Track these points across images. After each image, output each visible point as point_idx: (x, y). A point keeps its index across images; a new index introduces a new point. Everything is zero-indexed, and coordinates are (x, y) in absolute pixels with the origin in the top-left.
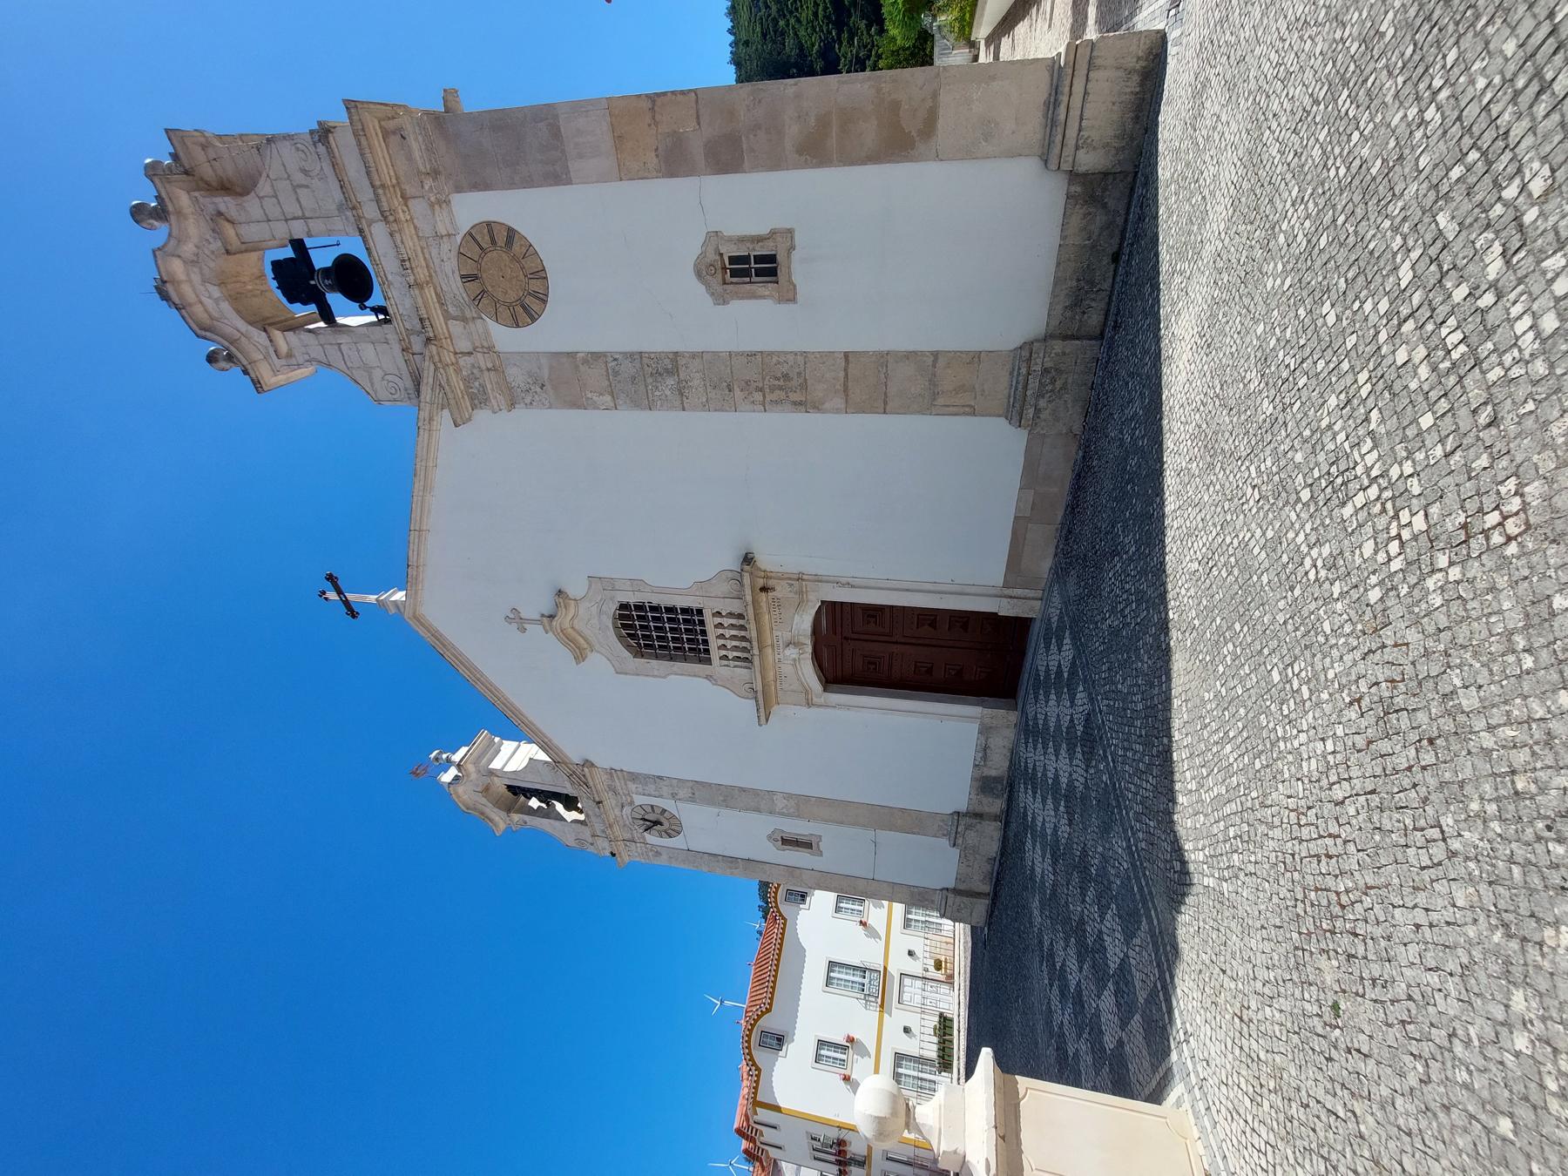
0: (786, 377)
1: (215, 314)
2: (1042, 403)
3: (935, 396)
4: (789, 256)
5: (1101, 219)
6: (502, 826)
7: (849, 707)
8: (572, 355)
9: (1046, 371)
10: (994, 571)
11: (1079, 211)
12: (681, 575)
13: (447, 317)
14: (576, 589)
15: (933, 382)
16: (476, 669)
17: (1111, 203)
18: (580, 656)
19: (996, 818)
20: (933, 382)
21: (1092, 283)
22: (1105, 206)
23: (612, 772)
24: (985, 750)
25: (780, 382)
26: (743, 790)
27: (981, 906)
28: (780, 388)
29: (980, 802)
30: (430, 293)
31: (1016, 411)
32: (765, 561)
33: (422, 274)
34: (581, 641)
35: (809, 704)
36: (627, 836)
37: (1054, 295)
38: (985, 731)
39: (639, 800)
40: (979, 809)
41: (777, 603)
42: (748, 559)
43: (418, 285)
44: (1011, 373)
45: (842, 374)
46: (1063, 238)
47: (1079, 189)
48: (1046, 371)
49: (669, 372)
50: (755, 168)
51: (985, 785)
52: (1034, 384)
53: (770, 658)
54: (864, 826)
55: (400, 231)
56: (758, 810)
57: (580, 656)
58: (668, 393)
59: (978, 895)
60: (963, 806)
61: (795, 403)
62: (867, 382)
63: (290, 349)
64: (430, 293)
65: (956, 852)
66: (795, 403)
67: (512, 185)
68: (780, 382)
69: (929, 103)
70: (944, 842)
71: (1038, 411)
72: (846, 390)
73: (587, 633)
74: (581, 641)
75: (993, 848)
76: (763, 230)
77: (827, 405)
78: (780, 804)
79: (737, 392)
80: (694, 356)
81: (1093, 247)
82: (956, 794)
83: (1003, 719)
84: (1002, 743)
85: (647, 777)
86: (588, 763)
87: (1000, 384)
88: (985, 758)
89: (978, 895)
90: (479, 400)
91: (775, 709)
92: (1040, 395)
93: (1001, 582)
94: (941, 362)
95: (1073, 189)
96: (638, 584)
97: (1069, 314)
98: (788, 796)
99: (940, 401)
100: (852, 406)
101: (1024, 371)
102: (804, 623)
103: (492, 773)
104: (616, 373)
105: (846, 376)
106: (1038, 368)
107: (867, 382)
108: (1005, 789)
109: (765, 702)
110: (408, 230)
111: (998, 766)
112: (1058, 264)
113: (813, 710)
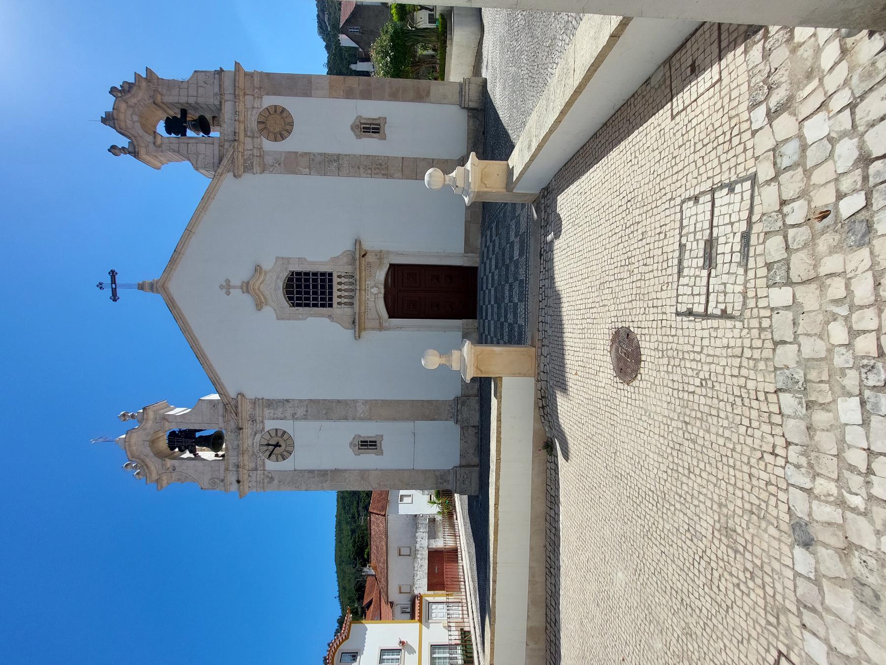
0: (381, 164)
5: (478, 123)
7: (400, 328)
8: (296, 153)
10: (458, 246)
11: (471, 120)
12: (320, 254)
13: (246, 136)
14: (267, 265)
16: (188, 324)
18: (259, 306)
23: (254, 402)
26: (339, 401)
32: (366, 246)
35: (381, 328)
39: (270, 425)
54: (408, 419)
56: (346, 418)
57: (259, 306)
63: (161, 144)
68: (379, 167)
85: (279, 401)
90: (248, 168)
96: (301, 260)
98: (366, 402)
102: (381, 275)
103: (165, 418)
104: (313, 160)
110: (242, 104)
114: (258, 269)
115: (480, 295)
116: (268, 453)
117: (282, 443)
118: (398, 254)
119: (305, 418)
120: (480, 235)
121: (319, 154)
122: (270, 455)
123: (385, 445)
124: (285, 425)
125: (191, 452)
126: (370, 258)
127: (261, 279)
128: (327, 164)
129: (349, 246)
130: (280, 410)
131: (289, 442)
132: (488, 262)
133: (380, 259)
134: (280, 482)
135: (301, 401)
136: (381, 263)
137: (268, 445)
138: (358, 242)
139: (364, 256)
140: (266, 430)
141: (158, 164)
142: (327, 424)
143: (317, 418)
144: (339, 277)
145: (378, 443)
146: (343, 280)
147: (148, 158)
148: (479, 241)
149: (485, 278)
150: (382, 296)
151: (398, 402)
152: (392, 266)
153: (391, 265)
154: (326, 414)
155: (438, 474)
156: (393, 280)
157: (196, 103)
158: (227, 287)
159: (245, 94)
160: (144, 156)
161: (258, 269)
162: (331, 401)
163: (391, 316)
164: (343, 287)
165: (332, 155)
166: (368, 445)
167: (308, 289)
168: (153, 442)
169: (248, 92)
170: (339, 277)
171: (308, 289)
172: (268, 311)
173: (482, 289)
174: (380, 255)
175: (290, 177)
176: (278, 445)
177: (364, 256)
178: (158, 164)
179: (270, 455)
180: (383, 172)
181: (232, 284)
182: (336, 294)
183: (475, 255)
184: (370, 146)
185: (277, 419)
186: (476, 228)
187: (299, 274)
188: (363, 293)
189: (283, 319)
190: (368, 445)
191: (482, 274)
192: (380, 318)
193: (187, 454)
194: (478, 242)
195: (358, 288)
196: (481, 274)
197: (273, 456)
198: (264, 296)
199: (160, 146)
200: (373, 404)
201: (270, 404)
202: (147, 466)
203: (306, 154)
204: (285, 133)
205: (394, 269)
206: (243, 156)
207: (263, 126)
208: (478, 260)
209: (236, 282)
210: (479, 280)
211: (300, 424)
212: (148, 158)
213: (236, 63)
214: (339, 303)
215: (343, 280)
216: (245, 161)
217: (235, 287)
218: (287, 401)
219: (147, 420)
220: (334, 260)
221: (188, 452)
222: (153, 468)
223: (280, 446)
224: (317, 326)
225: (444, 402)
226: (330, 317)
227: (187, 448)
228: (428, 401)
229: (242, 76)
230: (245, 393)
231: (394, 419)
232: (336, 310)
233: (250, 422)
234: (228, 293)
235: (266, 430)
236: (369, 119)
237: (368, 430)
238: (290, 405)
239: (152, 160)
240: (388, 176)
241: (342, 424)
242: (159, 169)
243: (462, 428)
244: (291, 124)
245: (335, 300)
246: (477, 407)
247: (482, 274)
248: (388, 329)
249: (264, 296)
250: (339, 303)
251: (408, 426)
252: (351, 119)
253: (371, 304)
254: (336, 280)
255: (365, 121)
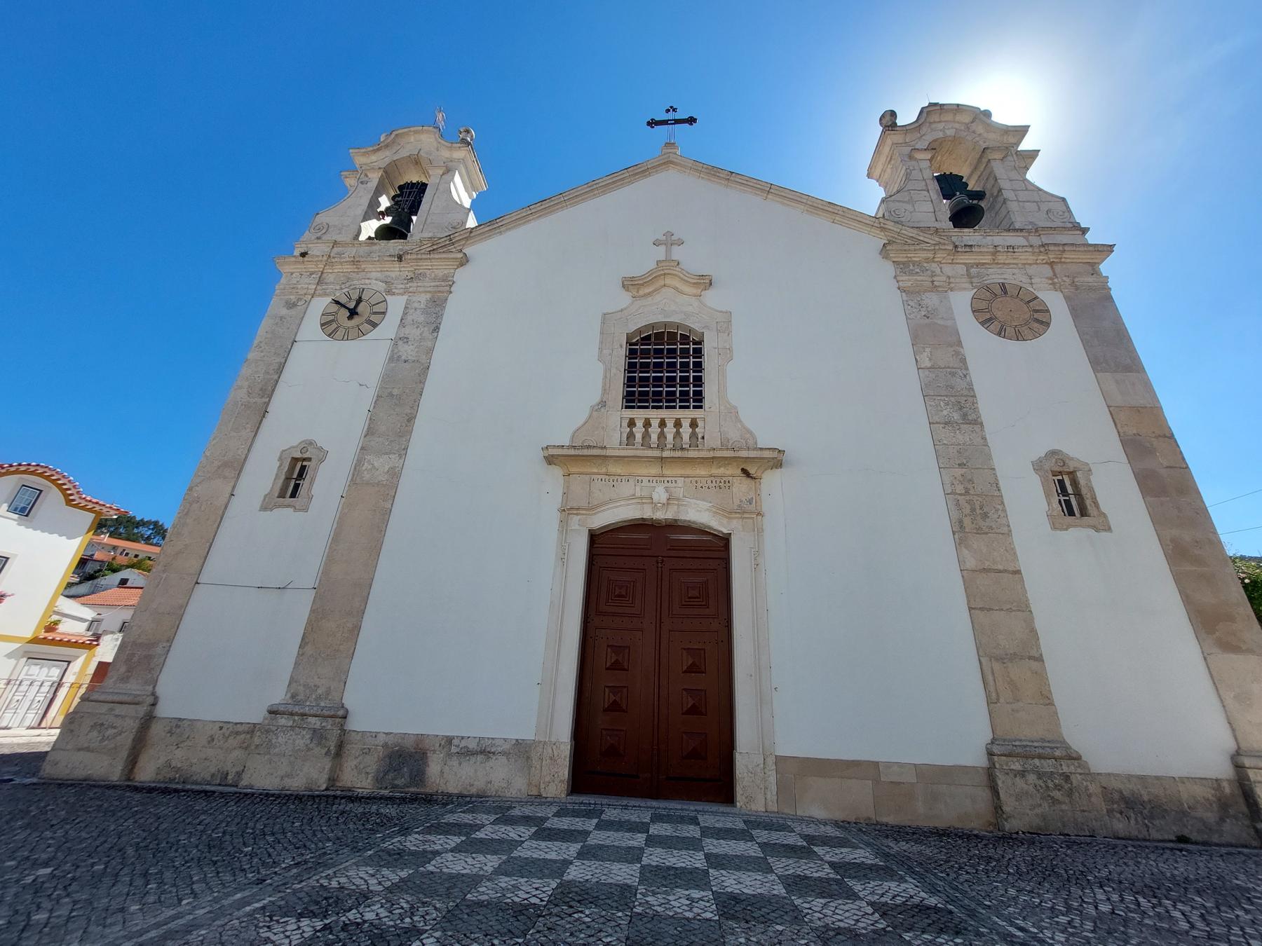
0: (985, 516)
1: (933, 126)
2: (1032, 778)
3: (993, 658)
4: (1089, 526)
5: (1211, 817)
6: (360, 160)
7: (563, 559)
8: (960, 343)
9: (1067, 778)
10: (792, 745)
11: (1209, 793)
12: (742, 390)
13: (969, 266)
14: (712, 298)
15: (1014, 657)
16: (604, 193)
17: (1227, 826)
18: (630, 284)
19: (332, 780)
20: (1014, 657)
21: (1152, 817)
22: (1222, 820)
23: (448, 282)
24: (484, 751)
25: (976, 512)
26: (411, 419)
27: (108, 767)
28: (973, 510)
29: (366, 752)
30: (987, 259)
31: (1000, 749)
32: (771, 481)
33: (1001, 258)
34: (647, 290)
35: (567, 511)
36: (330, 278)
37: (1142, 778)
38: (521, 751)
39: (396, 305)
40: (353, 750)
41: (727, 484)
42: (776, 461)
43: (994, 254)
44: (1043, 740)
45: (1000, 567)
46: (1183, 780)
47: (1227, 790)
48: (1067, 778)
49: (965, 416)
50: (1149, 507)
51: (406, 759)
52: (1048, 766)
53: (644, 471)
54: (326, 572)
55: (1034, 253)
56: (370, 432)
57: (630, 284)
58: (945, 413)
59: (133, 761)
60: (357, 723)
61: (961, 522)
62: (996, 596)
63: (916, 159)
64: (987, 259)
65: (257, 715)
66: (961, 522)
67: (1081, 334)
68: (976, 512)
69: (240, 768)
70: (278, 695)
71: (1022, 774)
72: (985, 570)
73: (658, 298)
74: (647, 290)
75: (263, 775)
76: (1103, 508)
77: (965, 552)
78: (382, 464)
79: (959, 471)
80: (984, 438)
81: (1184, 813)
82: (384, 704)
83: (555, 773)
84: (500, 777)
85: (439, 316)
86: (464, 261)
87: (1028, 731)
88: (467, 753)
89: (133, 761)
90: (903, 267)
91: (557, 471)
92: (1040, 776)
93: (780, 753)
94: (1034, 664)
95: (1225, 784)
96: (727, 353)
97: (1116, 796)
98: (395, 474)
99: (997, 666)
100: (970, 578)
101: (1057, 753)
102: (699, 512)
103: (449, 171)
104: (953, 374)
105: (1000, 571)
106: (1065, 769)
107: (996, 596)
108: (405, 793)
109: (569, 458)
110: (1031, 258)
111: (445, 775)
112: (1157, 778)
113: (556, 516)
114: (706, 283)
115: (638, 810)
116: (343, 300)
117: (356, 320)
118: (757, 553)
119: (394, 358)
120: (839, 816)
121: (970, 384)
122: (337, 302)
123: (286, 516)
124: (388, 328)
125: (387, 209)
126: (741, 487)
127: (687, 289)
128: (953, 404)
129: (766, 438)
130: (421, 319)
131: (353, 333)
132: (751, 849)
133: (741, 512)
134: (281, 318)
135: (430, 351)
136: (729, 513)
137: (359, 301)
138: (776, 461)
139: (744, 471)
140: (389, 298)
141: (877, 172)
142: (370, 395)
143: (388, 378)
144: (694, 424)
145: (288, 500)
146: (686, 430)
147: (886, 149)
148: (818, 812)
149: (692, 831)
150: (647, 513)
151: (375, 550)
152: (724, 542)
153: (725, 541)
154: (391, 395)
155: (159, 650)
156: (687, 545)
157: (1005, 201)
158: (669, 241)
159: (1051, 264)
160: (889, 142)
161: (706, 283)
162: (416, 405)
163: (594, 537)
164: (670, 430)
165: (976, 410)
166: (295, 477)
167: (663, 369)
168: (416, 161)
169: (1058, 268)
170: (694, 424)
171: (663, 369)
172: (624, 299)
173: (657, 818)
174: (751, 512)
175: (906, 338)
176: (353, 313)
177: (744, 471)
178: (877, 172)
179: (337, 302)
180: (967, 521)
181: (675, 248)
182: (655, 415)
183: (772, 794)
184: (1027, 502)
185: (405, 314)
186: (857, 800)
187: (698, 352)
188: (655, 470)
189: (603, 323)
190: (295, 477)
191: (708, 820)
192: (592, 509)
193: (385, 202)
194: (819, 805)
195: (666, 454)
196: (712, 816)
197: (335, 308)
198: (649, 294)
199: (911, 157)
200: (389, 488)
201: (437, 304)
202: (378, 150)
203: (963, 361)
204: (996, 326)
205: (716, 551)
206: (927, 260)
207: (998, 291)
208: (758, 806)
209: (677, 253)
210: (691, 808)
211: (384, 350)
212: (886, 149)
213: (1112, 246)
214: (632, 423)
215: (686, 430)
216: (919, 264)
217: (668, 252)
218: (437, 329)
219: (450, 148)
220: (733, 413)
221: (388, 204)
222: (374, 158)
223: (350, 318)
224: (584, 382)
225: (342, 677)
226: (603, 404)
227: (397, 203)
228: (356, 629)
229: (1086, 258)
230: (468, 267)
231: (336, 538)
232: (618, 415)
233: (410, 275)
234: (656, 243)
235: (389, 298)
236: (1091, 490)
237: (327, 485)
238: (427, 334)
239: (883, 159)
240: (961, 532)
241: (359, 424)
242: (869, 176)
243: (252, 729)
244: (1019, 337)
245: (639, 415)
246: (296, 784)
247: (708, 820)
248: (564, 523)
249: (649, 294)
250: (632, 423)
251: (309, 574)
252: (1076, 450)
253: (626, 489)
254: (686, 415)
255: (1082, 482)
